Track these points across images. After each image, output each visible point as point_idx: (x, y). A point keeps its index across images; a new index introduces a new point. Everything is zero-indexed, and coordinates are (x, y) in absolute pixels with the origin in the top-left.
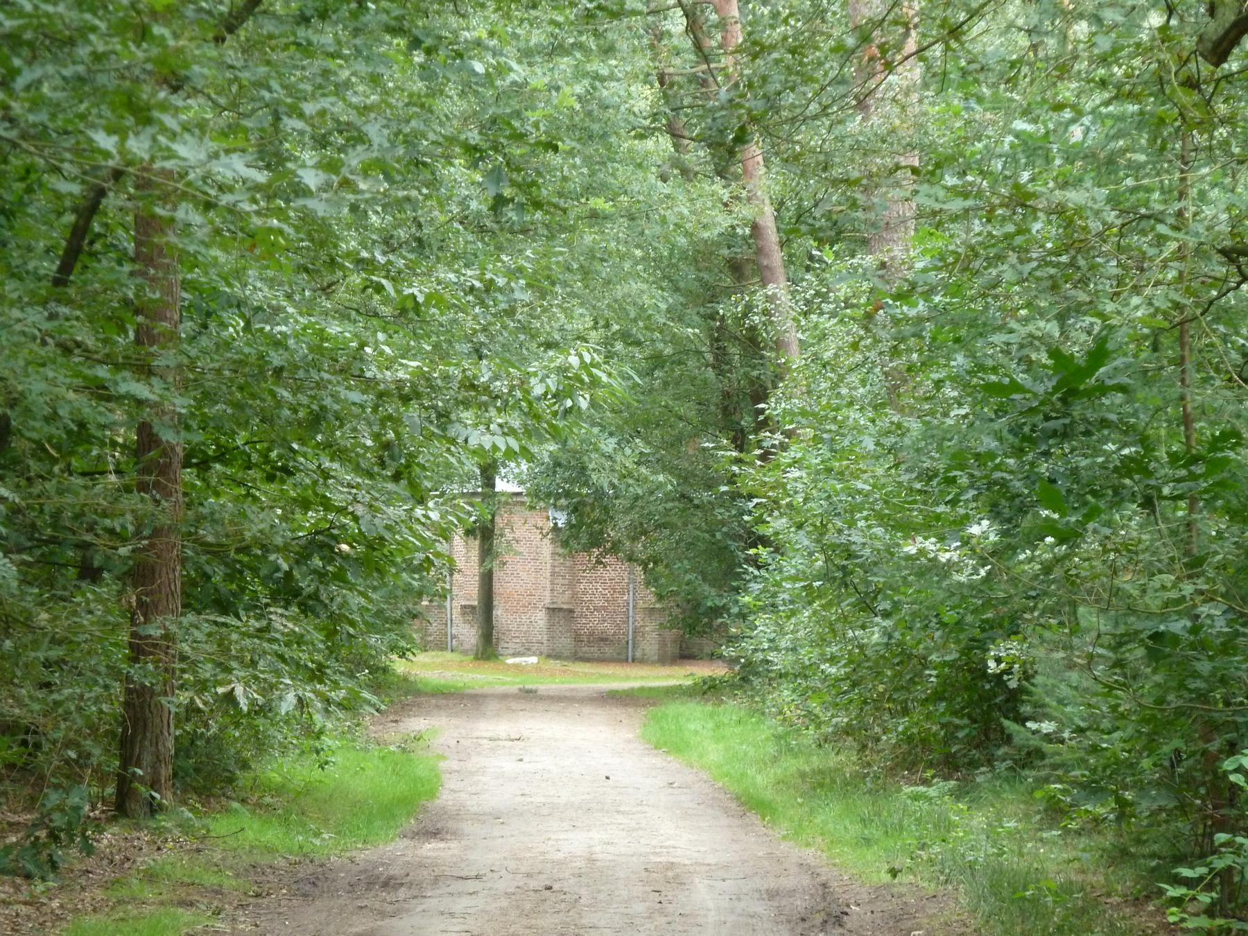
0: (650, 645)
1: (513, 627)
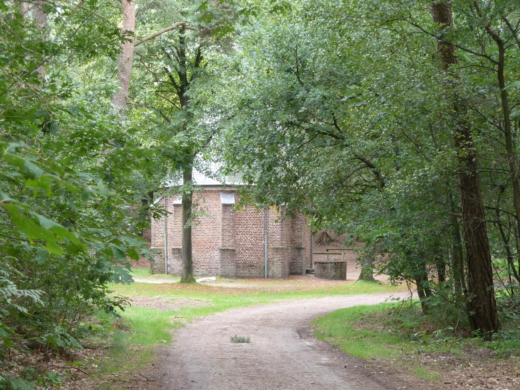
0: (277, 268)
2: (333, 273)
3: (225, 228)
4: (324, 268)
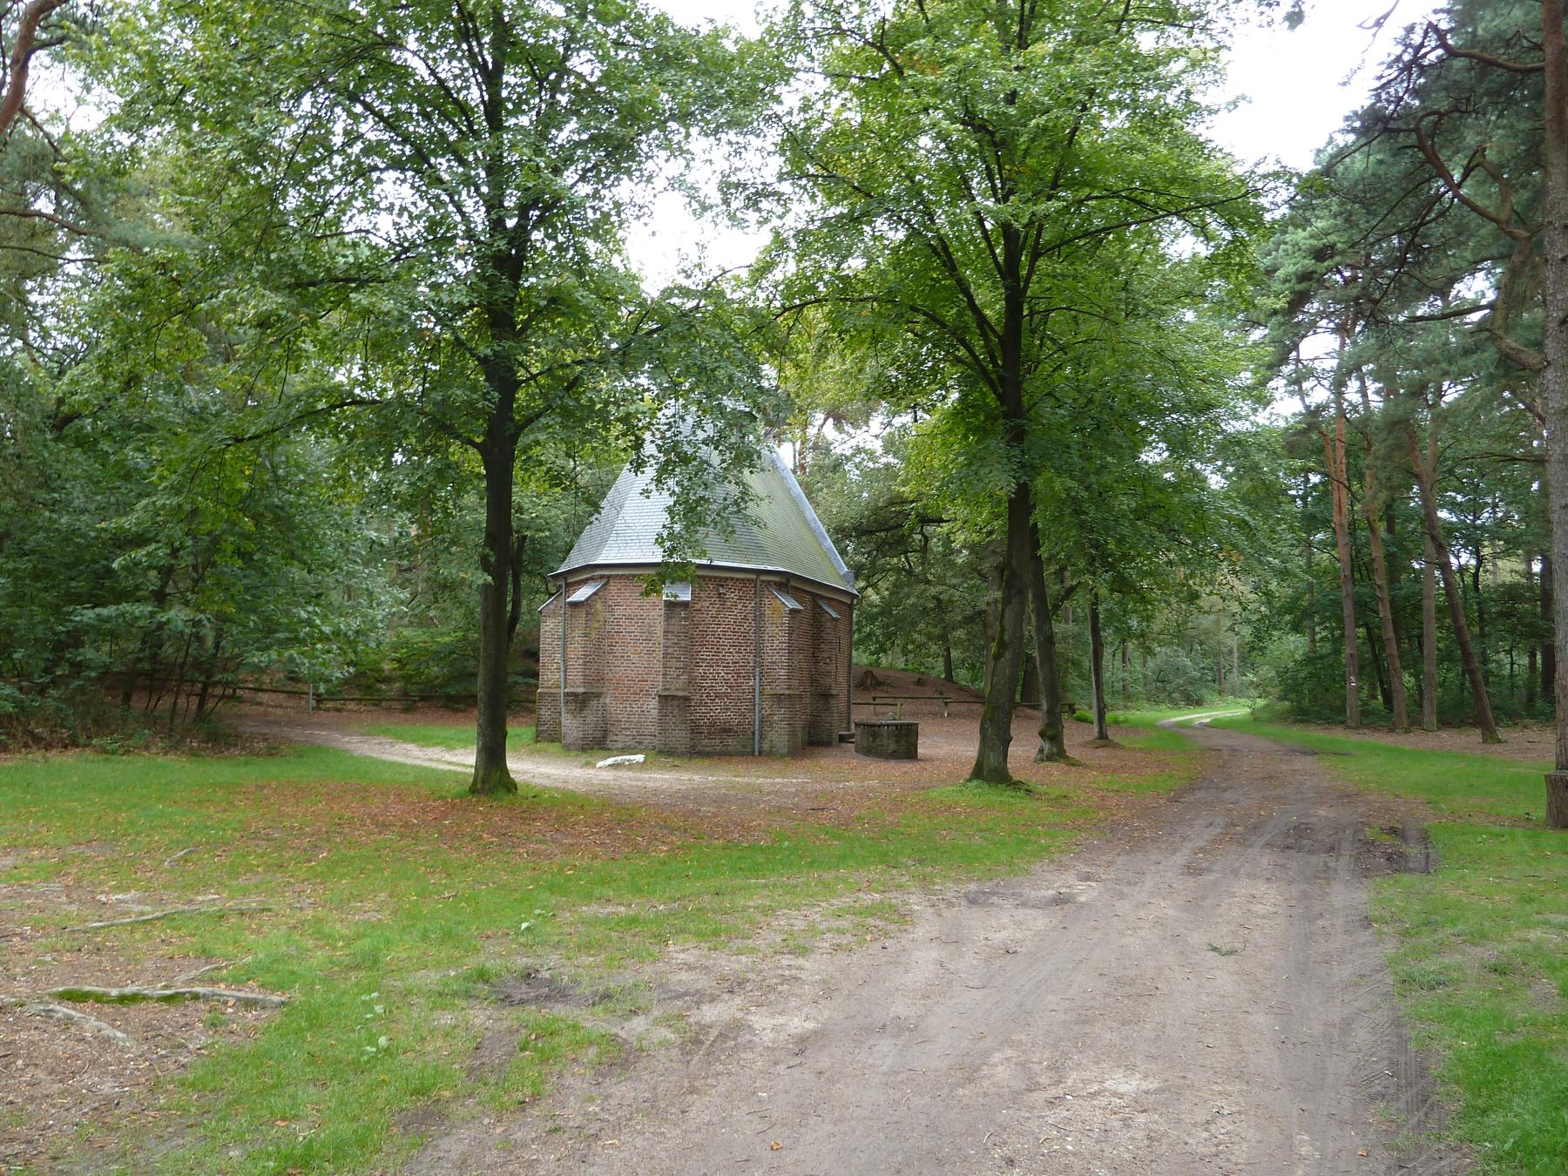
0: (779, 736)
1: (623, 717)
2: (893, 747)
3: (670, 650)
4: (875, 736)
